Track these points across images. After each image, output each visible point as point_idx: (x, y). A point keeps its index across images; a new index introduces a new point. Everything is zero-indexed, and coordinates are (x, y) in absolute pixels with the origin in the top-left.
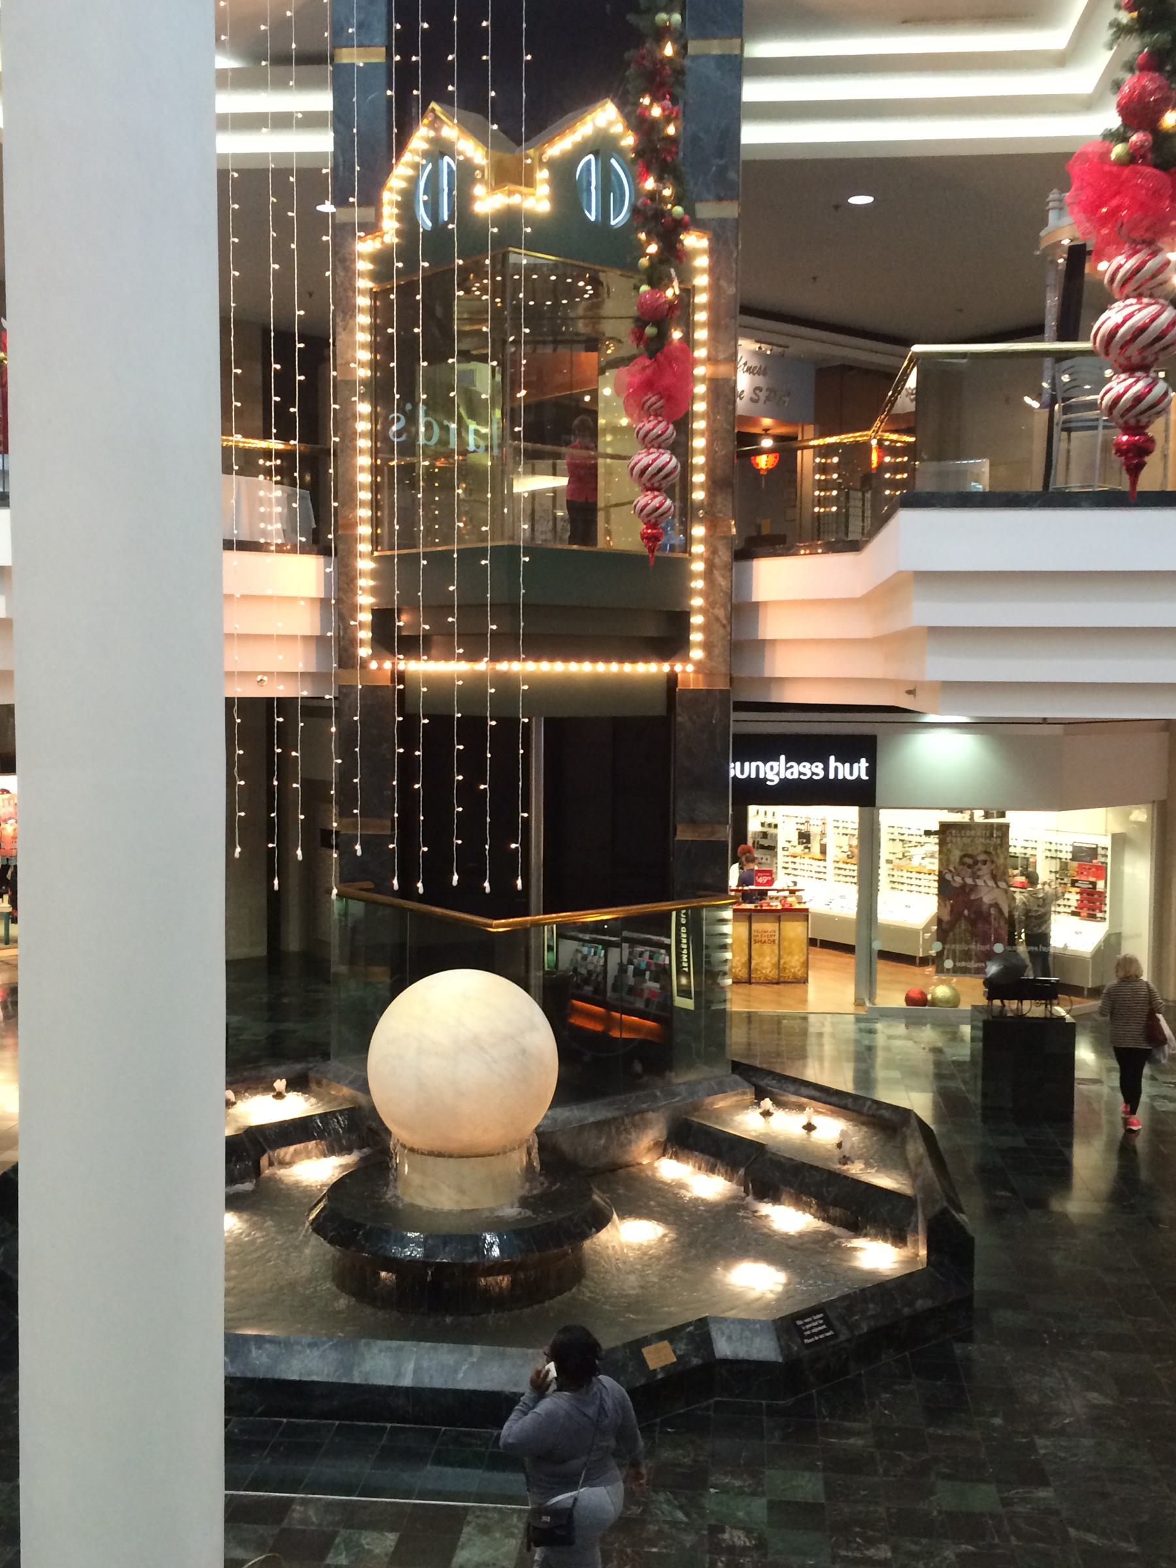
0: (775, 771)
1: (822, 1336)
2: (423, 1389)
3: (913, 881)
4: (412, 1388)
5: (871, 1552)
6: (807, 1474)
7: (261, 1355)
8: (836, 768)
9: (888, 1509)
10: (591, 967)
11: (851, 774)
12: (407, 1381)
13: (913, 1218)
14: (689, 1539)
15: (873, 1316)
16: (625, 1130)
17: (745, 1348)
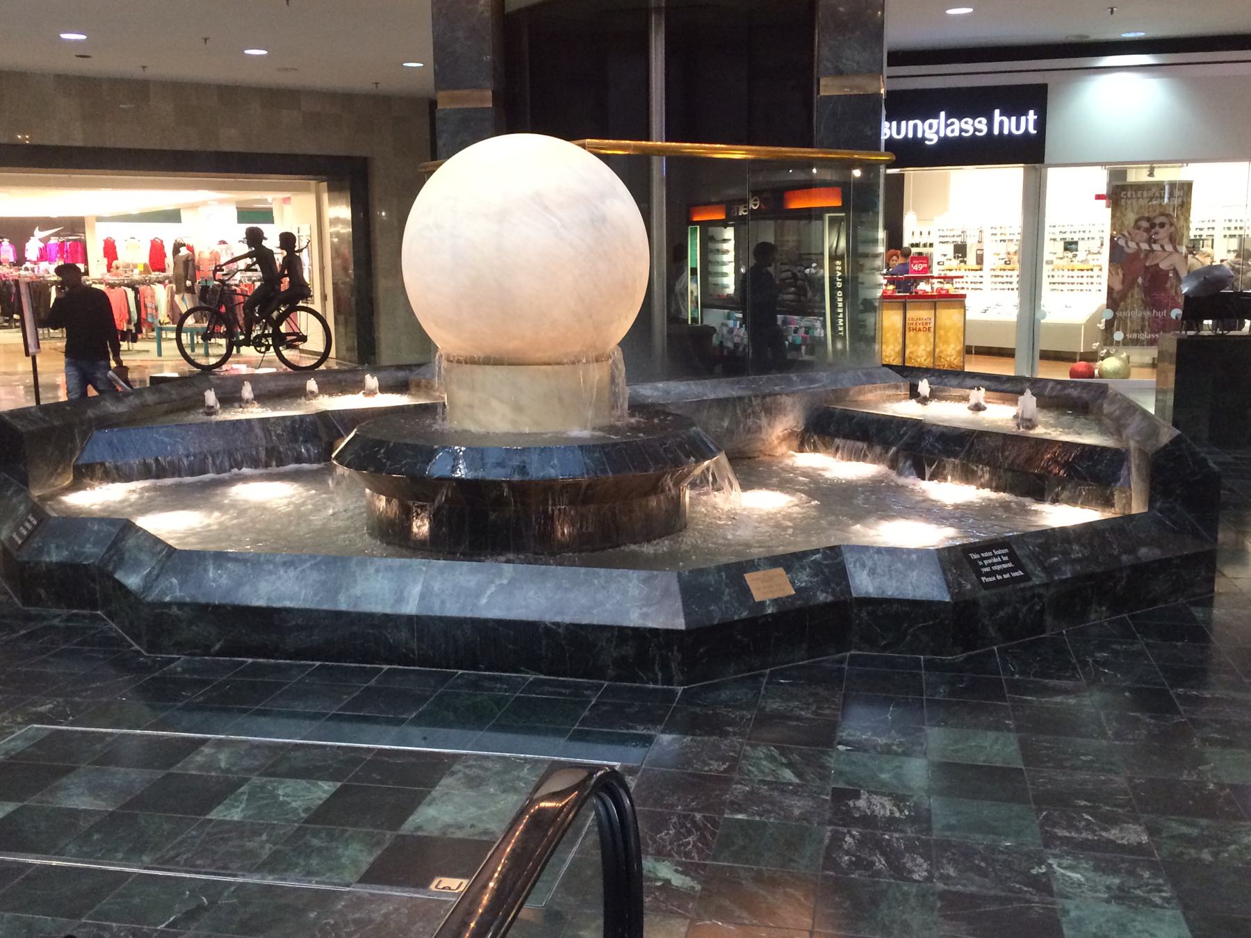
0: (933, 130)
1: (1007, 576)
3: (1075, 280)
4: (417, 616)
5: (1113, 834)
6: (992, 735)
7: (221, 576)
8: (1001, 123)
9: (1130, 780)
11: (1018, 128)
13: (1124, 472)
14: (798, 806)
15: (1078, 561)
16: (754, 413)
17: (894, 584)
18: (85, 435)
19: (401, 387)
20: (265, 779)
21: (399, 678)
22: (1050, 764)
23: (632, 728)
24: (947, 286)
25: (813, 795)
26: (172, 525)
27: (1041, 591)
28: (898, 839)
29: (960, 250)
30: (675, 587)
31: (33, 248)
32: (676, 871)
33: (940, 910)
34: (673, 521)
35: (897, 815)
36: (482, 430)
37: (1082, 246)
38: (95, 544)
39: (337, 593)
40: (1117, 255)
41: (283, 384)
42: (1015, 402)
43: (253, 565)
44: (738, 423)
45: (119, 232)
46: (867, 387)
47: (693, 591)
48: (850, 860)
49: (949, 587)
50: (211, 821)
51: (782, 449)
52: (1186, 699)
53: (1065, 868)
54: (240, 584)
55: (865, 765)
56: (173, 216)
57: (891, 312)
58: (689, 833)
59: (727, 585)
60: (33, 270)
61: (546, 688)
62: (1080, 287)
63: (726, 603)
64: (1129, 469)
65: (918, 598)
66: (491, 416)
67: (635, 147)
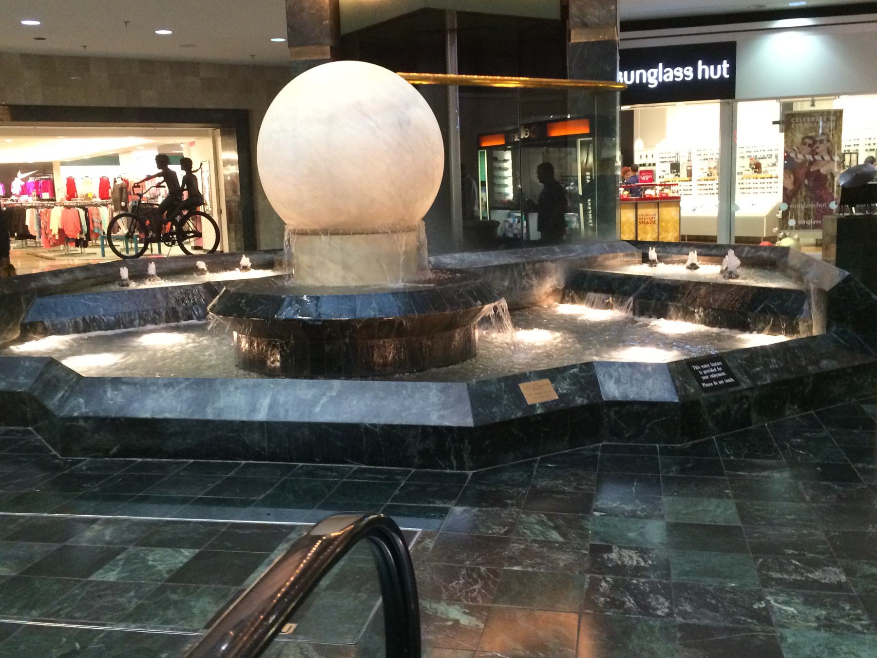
1: (721, 382)
2: (278, 423)
3: (759, 186)
4: (267, 422)
5: (817, 575)
6: (714, 502)
7: (117, 395)
8: (703, 71)
9: (827, 533)
10: (516, 231)
11: (715, 74)
12: (261, 416)
13: (806, 307)
16: (527, 275)
18: (29, 301)
19: (269, 265)
20: (139, 548)
21: (253, 470)
22: (762, 523)
23: (432, 503)
24: (666, 191)
25: (575, 550)
26: (87, 364)
27: (748, 393)
28: (643, 583)
29: (675, 167)
30: (466, 394)
31: (16, 186)
32: (465, 613)
33: (680, 639)
34: (468, 350)
35: (643, 564)
36: (320, 285)
37: (764, 163)
38: (26, 377)
39: (205, 407)
40: (790, 165)
41: (181, 264)
42: (720, 263)
43: (141, 386)
44: (515, 282)
45: (78, 173)
46: (611, 255)
47: (480, 398)
48: (606, 602)
49: (677, 391)
50: (92, 581)
51: (551, 300)
52: (864, 471)
53: (779, 603)
54: (130, 401)
55: (616, 526)
56: (113, 160)
57: (626, 211)
58: (476, 582)
59: (505, 392)
60: (17, 201)
61: (367, 475)
62: (762, 190)
63: (505, 406)
64: (810, 304)
65: (653, 400)
66: (328, 274)
67: (435, 79)
